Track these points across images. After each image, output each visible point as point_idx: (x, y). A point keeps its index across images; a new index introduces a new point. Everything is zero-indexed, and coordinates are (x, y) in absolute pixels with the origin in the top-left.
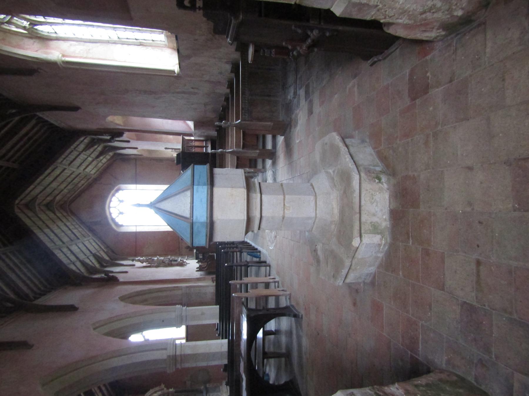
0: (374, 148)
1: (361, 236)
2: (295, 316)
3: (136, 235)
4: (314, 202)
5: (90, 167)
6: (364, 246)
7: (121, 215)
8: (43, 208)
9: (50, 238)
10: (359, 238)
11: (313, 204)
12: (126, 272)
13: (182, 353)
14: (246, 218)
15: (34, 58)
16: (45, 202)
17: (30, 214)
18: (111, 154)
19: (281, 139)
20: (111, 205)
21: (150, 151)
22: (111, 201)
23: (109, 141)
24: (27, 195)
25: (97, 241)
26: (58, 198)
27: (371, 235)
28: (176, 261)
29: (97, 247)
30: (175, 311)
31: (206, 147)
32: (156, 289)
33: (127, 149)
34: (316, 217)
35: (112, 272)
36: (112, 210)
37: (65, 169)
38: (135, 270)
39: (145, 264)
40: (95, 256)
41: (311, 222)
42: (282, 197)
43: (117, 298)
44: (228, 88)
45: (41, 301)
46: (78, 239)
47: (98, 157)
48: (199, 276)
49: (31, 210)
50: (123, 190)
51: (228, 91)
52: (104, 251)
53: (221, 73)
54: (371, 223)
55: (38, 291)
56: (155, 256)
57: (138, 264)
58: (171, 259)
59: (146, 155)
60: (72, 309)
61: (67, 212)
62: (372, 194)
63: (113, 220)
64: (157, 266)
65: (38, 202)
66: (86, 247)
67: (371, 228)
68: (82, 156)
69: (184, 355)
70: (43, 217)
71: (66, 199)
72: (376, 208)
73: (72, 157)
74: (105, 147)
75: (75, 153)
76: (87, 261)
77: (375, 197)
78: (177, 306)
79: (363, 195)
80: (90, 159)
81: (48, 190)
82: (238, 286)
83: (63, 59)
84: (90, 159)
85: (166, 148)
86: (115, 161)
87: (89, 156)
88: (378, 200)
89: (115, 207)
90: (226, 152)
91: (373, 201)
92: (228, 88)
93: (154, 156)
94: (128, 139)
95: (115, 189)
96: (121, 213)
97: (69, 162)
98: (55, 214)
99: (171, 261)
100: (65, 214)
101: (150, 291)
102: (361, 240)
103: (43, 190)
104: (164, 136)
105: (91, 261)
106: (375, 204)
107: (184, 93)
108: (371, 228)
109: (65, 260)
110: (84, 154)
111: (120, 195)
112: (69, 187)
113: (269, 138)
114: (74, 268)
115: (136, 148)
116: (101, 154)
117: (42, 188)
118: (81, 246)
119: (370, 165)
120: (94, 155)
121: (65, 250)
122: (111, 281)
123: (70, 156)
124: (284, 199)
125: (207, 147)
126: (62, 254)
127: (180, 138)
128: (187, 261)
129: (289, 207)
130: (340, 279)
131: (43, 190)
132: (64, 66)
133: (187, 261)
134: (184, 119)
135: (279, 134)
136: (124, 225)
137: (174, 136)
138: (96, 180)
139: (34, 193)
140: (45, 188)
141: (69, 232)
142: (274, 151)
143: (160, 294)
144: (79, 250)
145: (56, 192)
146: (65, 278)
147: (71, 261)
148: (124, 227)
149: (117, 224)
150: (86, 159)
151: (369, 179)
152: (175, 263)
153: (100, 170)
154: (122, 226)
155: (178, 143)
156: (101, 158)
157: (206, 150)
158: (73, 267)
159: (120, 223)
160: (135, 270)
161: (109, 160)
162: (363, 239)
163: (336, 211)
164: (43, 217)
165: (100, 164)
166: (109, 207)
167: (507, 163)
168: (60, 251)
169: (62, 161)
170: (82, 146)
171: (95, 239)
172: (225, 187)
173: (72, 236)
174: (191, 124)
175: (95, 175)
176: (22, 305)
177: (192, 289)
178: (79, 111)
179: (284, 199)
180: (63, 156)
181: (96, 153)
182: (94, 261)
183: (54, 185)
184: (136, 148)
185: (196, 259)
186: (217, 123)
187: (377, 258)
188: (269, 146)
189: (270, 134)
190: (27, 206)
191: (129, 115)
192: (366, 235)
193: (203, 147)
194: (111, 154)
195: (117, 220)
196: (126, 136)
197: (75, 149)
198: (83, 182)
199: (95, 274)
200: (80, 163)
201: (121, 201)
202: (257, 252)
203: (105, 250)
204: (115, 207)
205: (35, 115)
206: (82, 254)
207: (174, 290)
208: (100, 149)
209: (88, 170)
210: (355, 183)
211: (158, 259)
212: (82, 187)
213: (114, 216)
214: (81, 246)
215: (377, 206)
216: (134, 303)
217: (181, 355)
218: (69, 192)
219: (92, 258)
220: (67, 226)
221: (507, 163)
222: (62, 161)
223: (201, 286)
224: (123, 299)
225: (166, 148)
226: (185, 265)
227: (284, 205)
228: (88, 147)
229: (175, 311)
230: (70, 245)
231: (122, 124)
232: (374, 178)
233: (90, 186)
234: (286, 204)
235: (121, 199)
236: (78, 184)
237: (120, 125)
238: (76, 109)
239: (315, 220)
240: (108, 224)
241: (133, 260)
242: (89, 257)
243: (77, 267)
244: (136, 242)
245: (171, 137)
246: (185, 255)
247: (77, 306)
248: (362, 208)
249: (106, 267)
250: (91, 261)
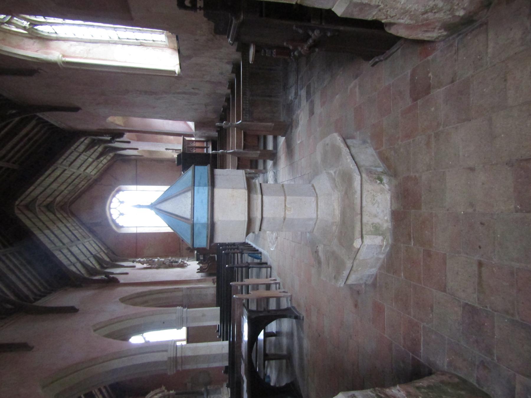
0: (375, 149)
1: (362, 237)
2: (296, 317)
3: (137, 236)
4: (315, 203)
5: (90, 167)
6: (365, 248)
7: (121, 216)
8: (43, 209)
9: (50, 240)
10: (360, 239)
11: (314, 205)
12: (127, 274)
13: (183, 355)
14: (247, 219)
15: (34, 58)
16: (45, 203)
17: (30, 215)
18: (112, 154)
19: (282, 140)
20: (112, 206)
21: (150, 152)
22: (111, 202)
23: (110, 141)
24: (28, 196)
25: (97, 242)
26: (58, 199)
27: (372, 236)
28: (177, 262)
29: (97, 248)
30: (176, 313)
31: (207, 148)
32: (156, 290)
33: (128, 150)
34: (317, 218)
35: (113, 273)
36: (112, 211)
37: (65, 170)
38: (135, 271)
39: (145, 265)
40: (95, 257)
41: (312, 223)
42: (283, 198)
43: (118, 299)
44: (228, 88)
45: (41, 303)
46: (79, 240)
47: (98, 158)
48: (199, 278)
49: (31, 211)
50: (123, 191)
51: (229, 91)
52: (104, 252)
53: (222, 73)
54: (372, 224)
55: (38, 293)
57: (139, 265)
58: (171, 260)
59: (146, 155)
60: (72, 310)
61: (67, 213)
62: (374, 195)
63: (114, 221)
64: (158, 268)
65: (38, 203)
66: (87, 248)
67: (372, 229)
68: (83, 157)
69: (185, 357)
70: (43, 218)
72: (378, 209)
73: (72, 158)
74: (106, 148)
75: (76, 154)
76: (88, 262)
78: (178, 307)
79: (364, 196)
80: (90, 160)
81: (49, 191)
82: (239, 288)
83: (64, 59)
84: (90, 160)
85: (167, 149)
86: (115, 162)
87: (90, 157)
88: (379, 201)
89: (115, 208)
90: (226, 153)
91: (374, 202)
92: (228, 88)
93: (155, 156)
94: (128, 140)
95: (116, 189)
96: (122, 214)
97: (69, 163)
98: (55, 215)
99: (172, 262)
100: (65, 215)
101: (151, 293)
102: (362, 242)
103: (43, 191)
104: (165, 137)
105: (91, 262)
106: (376, 205)
107: (185, 93)
108: (372, 229)
109: (65, 262)
110: (84, 155)
111: (120, 196)
112: (69, 188)
113: (270, 138)
114: (74, 269)
115: (137, 149)
116: (102, 154)
117: (42, 189)
118: (81, 247)
119: (372, 166)
120: (94, 156)
121: (65, 251)
122: (112, 282)
123: (70, 157)
124: (285, 200)
125: (208, 148)
126: (62, 255)
127: (181, 138)
128: (188, 263)
129: (291, 208)
131: (43, 191)
132: (64, 66)
133: (188, 263)
134: (185, 119)
135: (280, 135)
136: (124, 226)
137: (175, 137)
138: (96, 181)
139: (34, 194)
140: (45, 189)
141: (69, 234)
142: (275, 151)
143: (161, 296)
144: (79, 251)
145: (57, 193)
146: (65, 279)
147: (72, 263)
148: (124, 229)
149: (117, 226)
150: (87, 160)
151: (370, 180)
152: (176, 264)
153: (100, 171)
154: (122, 227)
155: (178, 143)
156: (102, 158)
157: (207, 150)
158: (73, 269)
159: (121, 224)
160: (135, 271)
161: (109, 161)
162: (364, 240)
163: (337, 212)
164: (43, 218)
165: (101, 165)
166: (110, 208)
167: (509, 163)
168: (60, 253)
169: (62, 162)
170: (82, 147)
171: (95, 240)
172: (226, 188)
173: (73, 237)
174: (192, 124)
175: (96, 176)
177: (193, 291)
178: (80, 111)
179: (285, 200)
180: (63, 157)
181: (97, 154)
182: (94, 262)
183: (54, 186)
184: (137, 149)
185: (197, 260)
186: (218, 124)
187: (378, 259)
188: (270, 147)
189: (271, 135)
190: (27, 207)
191: (130, 116)
192: (367, 236)
193: (203, 148)
194: (112, 154)
195: (118, 221)
196: (126, 137)
197: (75, 149)
198: (83, 183)
199: (95, 275)
200: (80, 164)
201: (122, 202)
202: (258, 253)
203: (106, 251)
204: (115, 208)
205: (35, 116)
206: (82, 256)
207: (175, 291)
208: (100, 149)
209: (89, 170)
210: (357, 184)
211: (158, 260)
212: (83, 188)
213: (114, 217)
214: (81, 247)
215: (378, 207)
216: (135, 304)
217: (182, 357)
218: (69, 193)
219: (92, 259)
220: (67, 227)
221: (509, 163)
222: (62, 162)
223: (202, 288)
224: (123, 300)
225: (167, 149)
226: (186, 266)
227: (285, 206)
228: (89, 147)
229: (176, 313)
230: (70, 246)
232: (375, 178)
233: (90, 187)
234: (287, 205)
235: (121, 200)
236: (78, 185)
237: (121, 126)
238: (76, 109)
239: (316, 221)
240: (109, 225)
241: (133, 262)
242: (90, 259)
243: (77, 269)
244: (136, 243)
245: (172, 137)
246: (186, 256)
247: (77, 307)
248: (364, 209)
249: (106, 268)
250: (91, 262)
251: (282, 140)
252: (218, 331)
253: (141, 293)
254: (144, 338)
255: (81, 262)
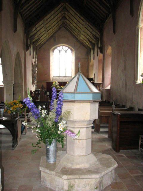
0: (110, 185)
1: (67, 179)
2: (13, 146)
4: (82, 155)
5: (84, 37)
6: (62, 181)
8: (63, 15)
10: (67, 178)
11: (82, 154)
12: (30, 55)
14: (75, 120)
15: (139, 16)
16: (66, 16)
18: (91, 47)
19: (106, 136)
20: (64, 47)
21: (92, 66)
22: (66, 46)
23: (98, 46)
24: (70, 8)
26: (68, 22)
27: (68, 185)
29: (43, 40)
30: (11, 80)
32: (22, 70)
34: (74, 156)
35: (31, 48)
36: (61, 47)
37: (83, 25)
38: (31, 59)
39: (34, 64)
41: (72, 153)
42: (85, 138)
43: (19, 51)
44: (130, 107)
45: (19, 15)
46: (48, 31)
47: (89, 40)
50: (72, 52)
51: (128, 107)
53: (137, 104)
54: (74, 185)
55: (23, 13)
56: (37, 69)
57: (34, 60)
58: (36, 77)
59: (91, 64)
60: (15, 30)
61: (61, 25)
62: (88, 185)
63: (56, 48)
64: (32, 70)
65: (66, 13)
67: (71, 185)
68: (89, 33)
70: (60, 14)
71: (65, 24)
72: (82, 187)
73: (89, 29)
74: (94, 44)
75: (91, 30)
76: (36, 36)
77: (87, 186)
78: (14, 81)
79: (88, 180)
80: (88, 37)
81: (72, 18)
82: (24, 114)
83: (140, 28)
84: (88, 37)
85: (94, 74)
86: (87, 48)
87: (89, 36)
88: (86, 188)
89: (63, 48)
91: (85, 185)
92: (130, 107)
93: (90, 68)
94: (99, 56)
95: (73, 49)
96: (60, 51)
97: (86, 27)
101: (21, 67)
102: (65, 180)
103: (72, 15)
104: (101, 74)
105: (36, 37)
106: (84, 186)
107: (126, 85)
108: (71, 185)
110: (90, 34)
111: (69, 51)
112: (73, 27)
113: (107, 130)
114: (33, 30)
115: (94, 59)
116: (91, 42)
118: (44, 32)
119: (103, 183)
120: (90, 39)
121: (42, 25)
122: (27, 48)
123: (78, 17)
124: (83, 140)
126: (41, 24)
127: (101, 82)
129: (80, 142)
130: (44, 169)
131: (72, 15)
132: (136, 28)
134: (112, 83)
135: (109, 135)
136: (54, 53)
137: (101, 79)
138: (77, 39)
139: (71, 11)
140: (73, 16)
141: (53, 25)
142: (99, 132)
143: (19, 72)
145: (71, 21)
146: (29, 25)
148: (52, 53)
149: (54, 49)
150: (88, 35)
151: (96, 183)
153: (82, 41)
154: (53, 52)
155: (98, 81)
156: (89, 42)
158: (34, 29)
159: (55, 51)
160: (31, 59)
161: (87, 45)
162: (66, 181)
163: (78, 166)
164: (60, 14)
165: (85, 42)
168: (42, 23)
169: (87, 24)
170: (94, 33)
171: (47, 39)
172: (90, 109)
174: (109, 87)
176: (17, 5)
178: (113, 33)
179: (83, 140)
180: (89, 25)
181: (91, 40)
182: (36, 39)
184: (94, 59)
185: (35, 90)
186: (114, 103)
187: (55, 188)
188: (102, 130)
189: (109, 130)
190: (65, 8)
191: (112, 57)
192: (68, 182)
194: (91, 47)
195: (56, 50)
196: (101, 55)
197: (93, 30)
198: (76, 33)
199: (30, 40)
200: (85, 32)
201: (66, 51)
204: (63, 48)
205: (110, 14)
206: (40, 33)
208: (93, 42)
209: (82, 36)
210: (94, 176)
212: (73, 33)
213: (58, 48)
214: (44, 32)
215: (83, 187)
216: (16, 59)
218: (71, 27)
219: (38, 38)
220: (54, 26)
222: (87, 24)
223: (22, 93)
224: (18, 54)
225: (94, 74)
227: (81, 140)
228: (95, 37)
229: (11, 80)
231: (107, 53)
232: (97, 185)
233: (74, 36)
234: (81, 141)
235: (67, 51)
236: (75, 31)
237: (106, 52)
238: (114, 32)
239: (73, 156)
240: (54, 46)
241: (36, 58)
243: (34, 31)
244: (44, 59)
245: (101, 77)
246: (37, 84)
247: (16, 32)
248: (82, 180)
249: (33, 45)
250: (36, 37)
251: (106, 136)
252: (2, 102)
253: (21, 61)
254: (61, 50)
255: (39, 39)
